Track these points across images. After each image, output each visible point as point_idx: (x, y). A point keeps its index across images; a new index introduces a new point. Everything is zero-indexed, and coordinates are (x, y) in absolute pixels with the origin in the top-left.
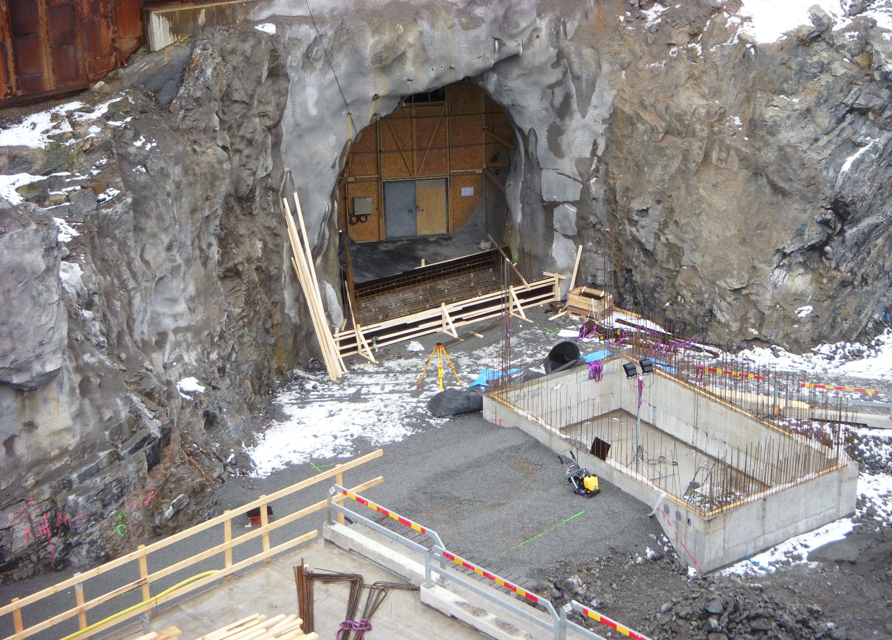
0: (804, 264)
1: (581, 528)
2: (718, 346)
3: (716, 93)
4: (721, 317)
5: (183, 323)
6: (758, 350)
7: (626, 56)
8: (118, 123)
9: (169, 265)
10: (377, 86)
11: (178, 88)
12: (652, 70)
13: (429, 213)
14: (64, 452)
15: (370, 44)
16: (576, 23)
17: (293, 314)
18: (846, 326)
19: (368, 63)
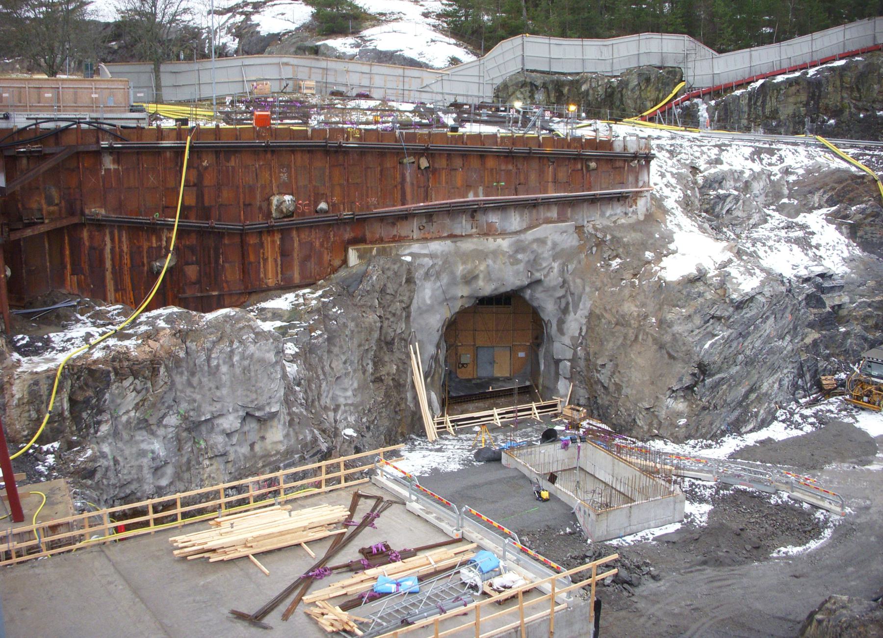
0: (684, 397)
1: (536, 514)
2: (637, 438)
3: (643, 305)
4: (640, 423)
5: (349, 402)
6: (657, 441)
7: (599, 284)
8: (326, 300)
9: (344, 371)
10: (463, 291)
11: (359, 285)
12: (611, 292)
13: (501, 367)
14: (278, 453)
15: (460, 269)
16: (574, 266)
17: (412, 405)
18: (704, 431)
19: (458, 279)
